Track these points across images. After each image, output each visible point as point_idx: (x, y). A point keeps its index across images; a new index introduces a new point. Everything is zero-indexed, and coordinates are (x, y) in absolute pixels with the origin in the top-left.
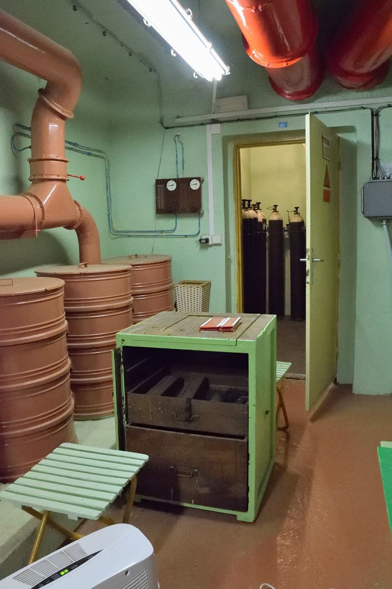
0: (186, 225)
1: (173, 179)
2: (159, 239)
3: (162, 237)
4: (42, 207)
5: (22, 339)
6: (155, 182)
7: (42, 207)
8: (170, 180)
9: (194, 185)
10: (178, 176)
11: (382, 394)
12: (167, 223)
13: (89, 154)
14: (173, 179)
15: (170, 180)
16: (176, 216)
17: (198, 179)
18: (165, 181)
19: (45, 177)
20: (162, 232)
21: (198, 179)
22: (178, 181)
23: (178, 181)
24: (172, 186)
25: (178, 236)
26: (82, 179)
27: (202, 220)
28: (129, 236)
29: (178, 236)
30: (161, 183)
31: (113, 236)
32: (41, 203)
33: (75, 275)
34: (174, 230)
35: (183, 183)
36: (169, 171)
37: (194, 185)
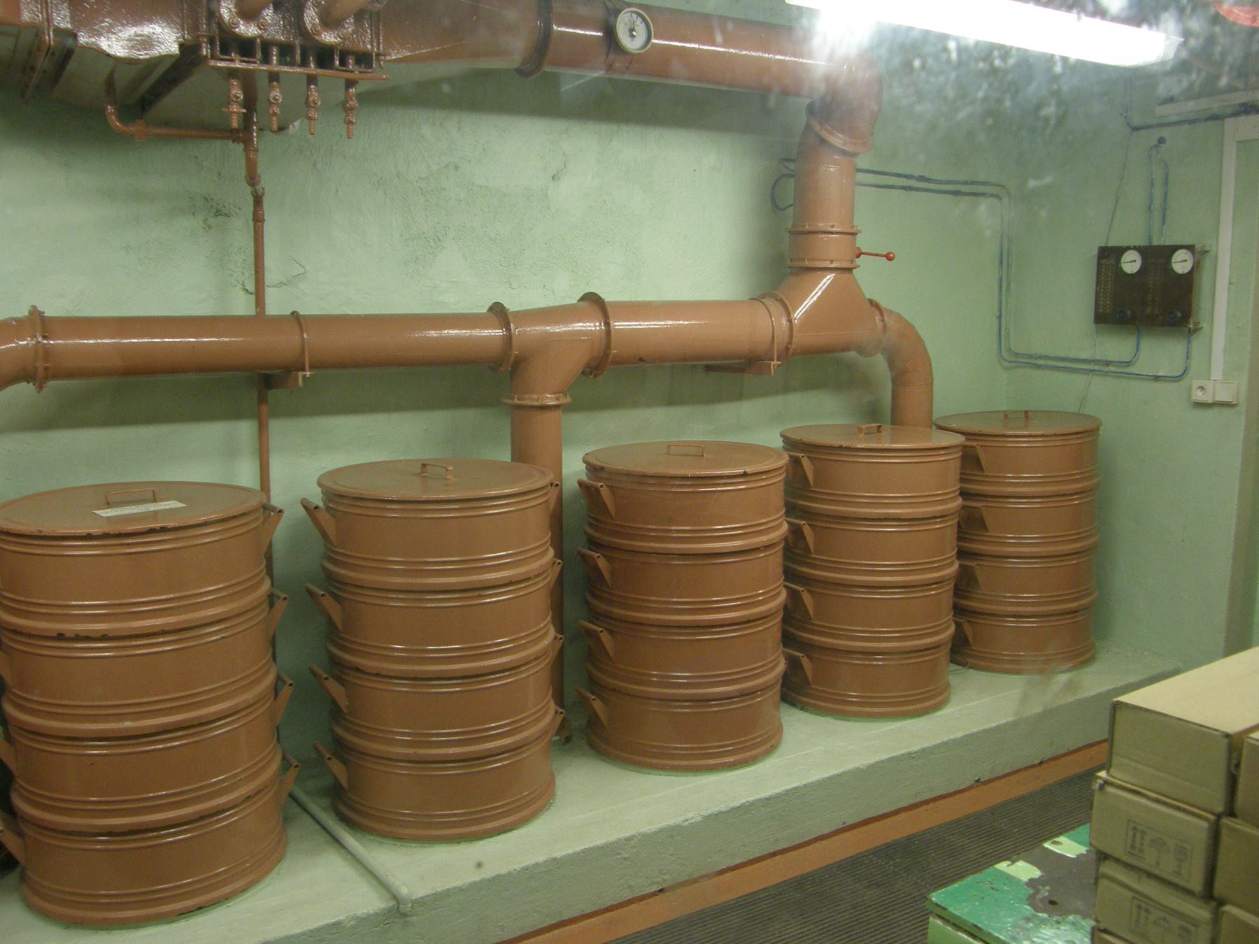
0: (1159, 353)
1: (1135, 248)
2: (1096, 380)
3: (1106, 374)
4: (790, 321)
5: (475, 578)
6: (1095, 252)
7: (790, 321)
8: (1128, 248)
9: (1181, 263)
10: (1150, 239)
11: (420, 893)
12: (1116, 346)
13: (956, 193)
14: (1135, 248)
15: (1128, 248)
16: (1139, 331)
17: (1190, 248)
18: (1120, 251)
19: (807, 264)
20: (1108, 363)
21: (1190, 248)
22: (1148, 253)
23: (1148, 253)
24: (1131, 264)
25: (1139, 377)
26: (889, 257)
27: (1197, 343)
28: (1038, 367)
29: (1139, 377)
30: (1109, 256)
31: (1006, 364)
32: (789, 314)
33: (831, 448)
34: (1129, 364)
35: (1157, 256)
36: (1130, 230)
37: (1181, 263)
